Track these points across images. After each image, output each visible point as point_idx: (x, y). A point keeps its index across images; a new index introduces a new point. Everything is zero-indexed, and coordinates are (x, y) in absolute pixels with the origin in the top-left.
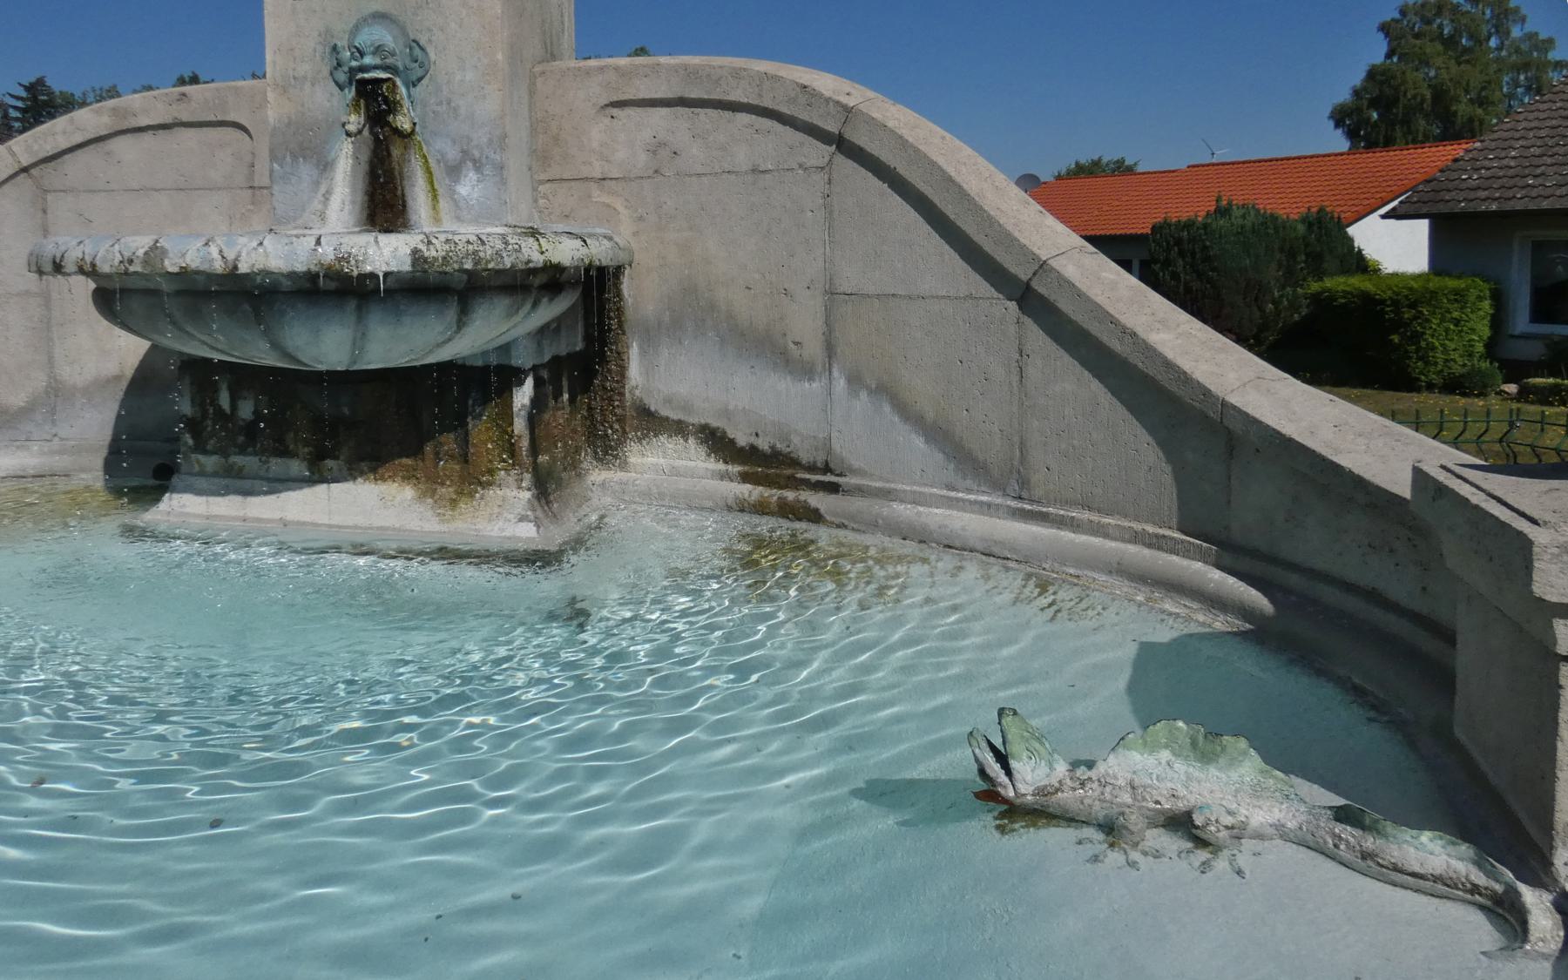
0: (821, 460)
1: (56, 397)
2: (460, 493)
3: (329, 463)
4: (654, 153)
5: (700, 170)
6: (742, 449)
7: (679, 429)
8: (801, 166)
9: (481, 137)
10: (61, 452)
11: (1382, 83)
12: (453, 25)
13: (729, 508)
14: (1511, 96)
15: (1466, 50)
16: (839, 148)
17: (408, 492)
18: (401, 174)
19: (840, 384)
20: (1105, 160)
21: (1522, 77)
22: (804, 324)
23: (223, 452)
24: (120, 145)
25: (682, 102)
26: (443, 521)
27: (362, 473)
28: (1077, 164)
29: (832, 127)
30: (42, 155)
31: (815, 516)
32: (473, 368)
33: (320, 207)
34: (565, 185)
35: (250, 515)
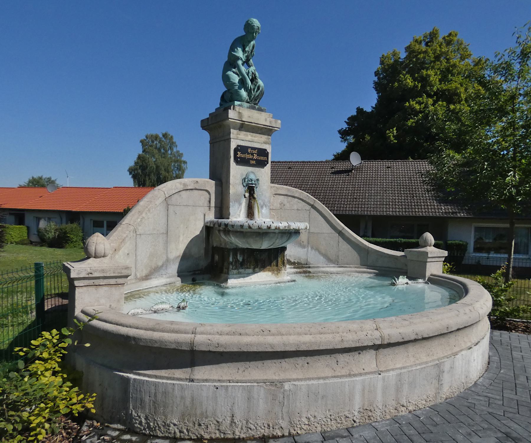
1: (168, 260)
3: (256, 269)
10: (169, 277)
15: (164, 154)
17: (270, 273)
19: (310, 249)
20: (44, 177)
28: (33, 178)
29: (312, 203)
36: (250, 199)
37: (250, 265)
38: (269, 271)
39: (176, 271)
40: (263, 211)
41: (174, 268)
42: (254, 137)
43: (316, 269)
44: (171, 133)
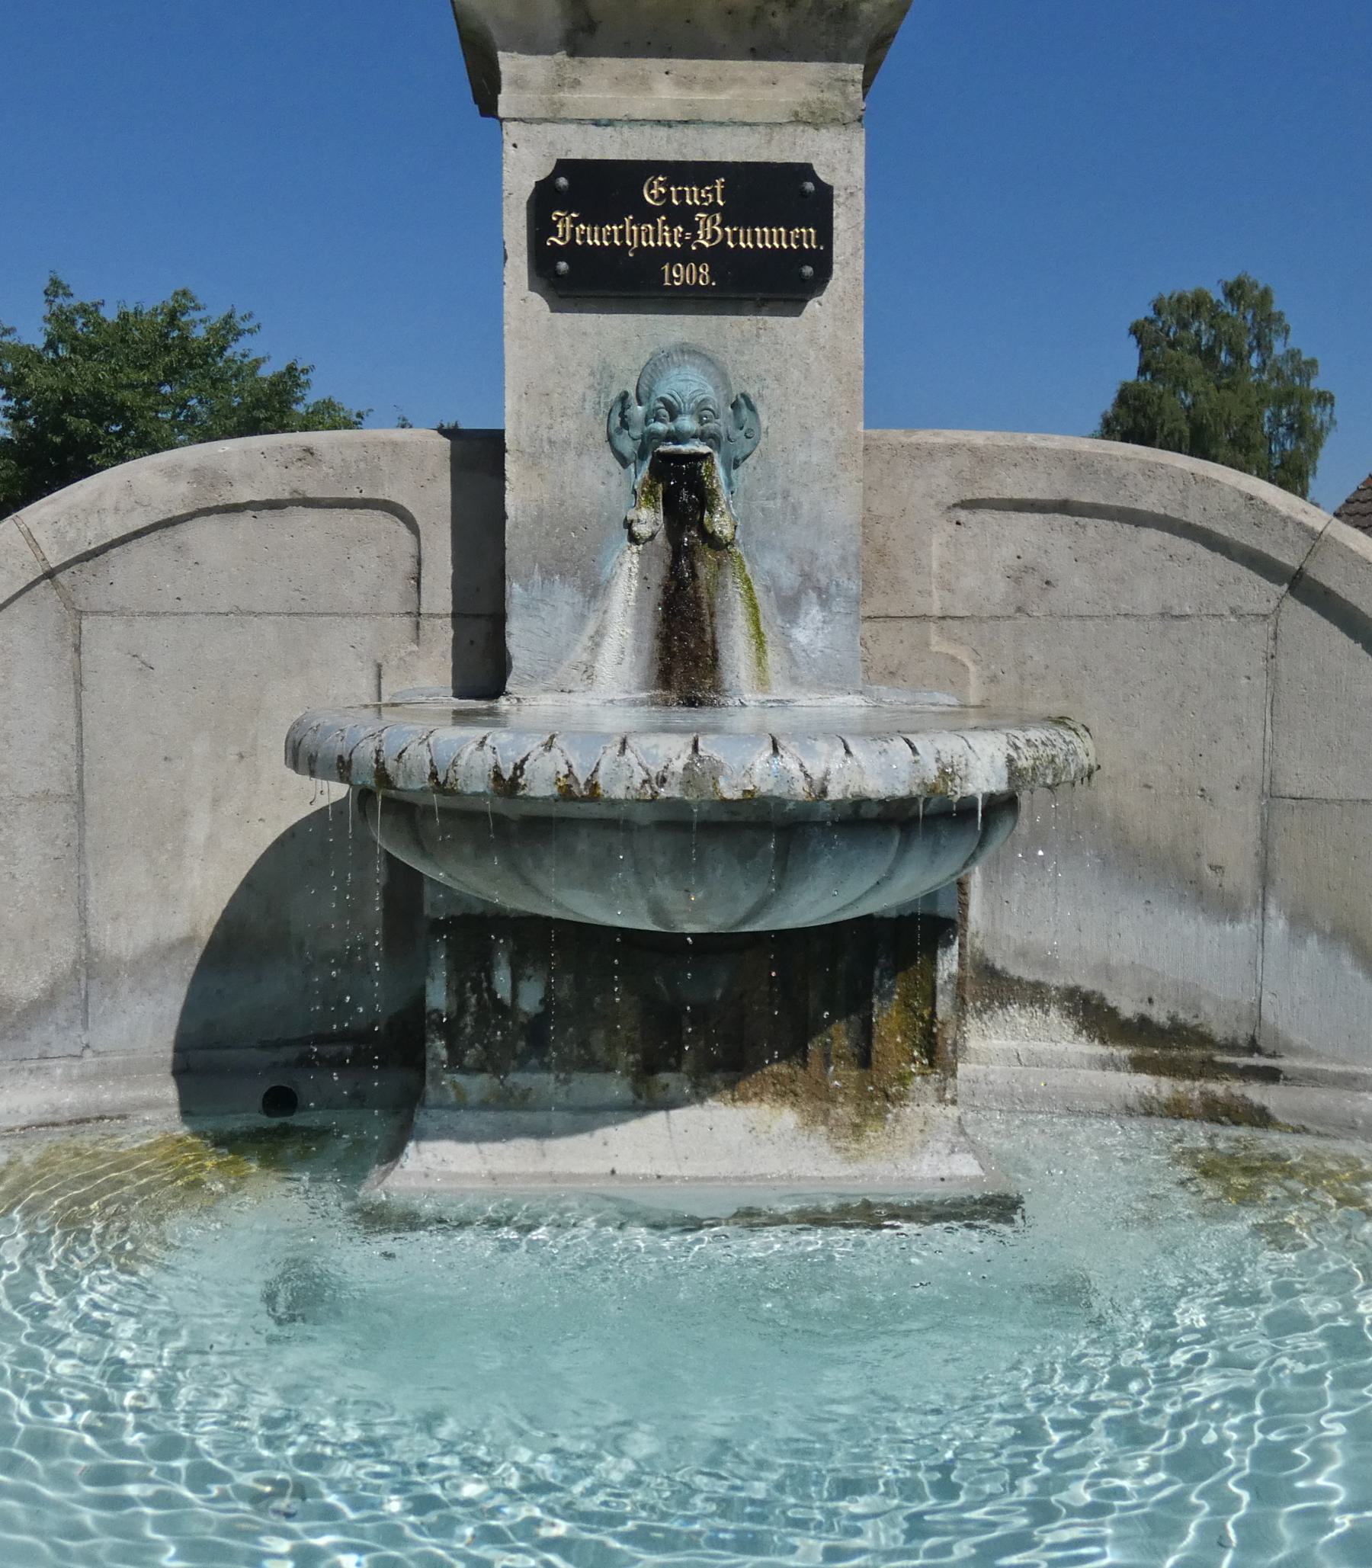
0: (1243, 1034)
1: (91, 971)
2: (864, 1114)
3: (665, 1077)
4: (1018, 580)
5: (1085, 610)
6: (1128, 1021)
7: (1035, 994)
8: (1233, 611)
9: (830, 552)
10: (102, 1074)
11: (1137, 410)
12: (796, 374)
13: (1130, 1111)
14: (1270, 438)
15: (1229, 370)
16: (1292, 590)
17: (787, 1118)
18: (711, 606)
19: (1278, 926)
21: (1284, 412)
22: (1229, 842)
23: (489, 1064)
24: (203, 534)
25: (1064, 507)
26: (849, 1160)
27: (714, 1091)
29: (1290, 559)
30: (82, 548)
31: (1261, 1118)
32: (890, 919)
33: (585, 657)
34: (893, 624)
35: (556, 1170)
36: (678, 551)
37: (610, 1048)
38: (785, 1093)
39: (170, 1036)
40: (801, 635)
41: (148, 1021)
42: (709, 85)
43: (1320, 1098)
44: (1260, 277)
